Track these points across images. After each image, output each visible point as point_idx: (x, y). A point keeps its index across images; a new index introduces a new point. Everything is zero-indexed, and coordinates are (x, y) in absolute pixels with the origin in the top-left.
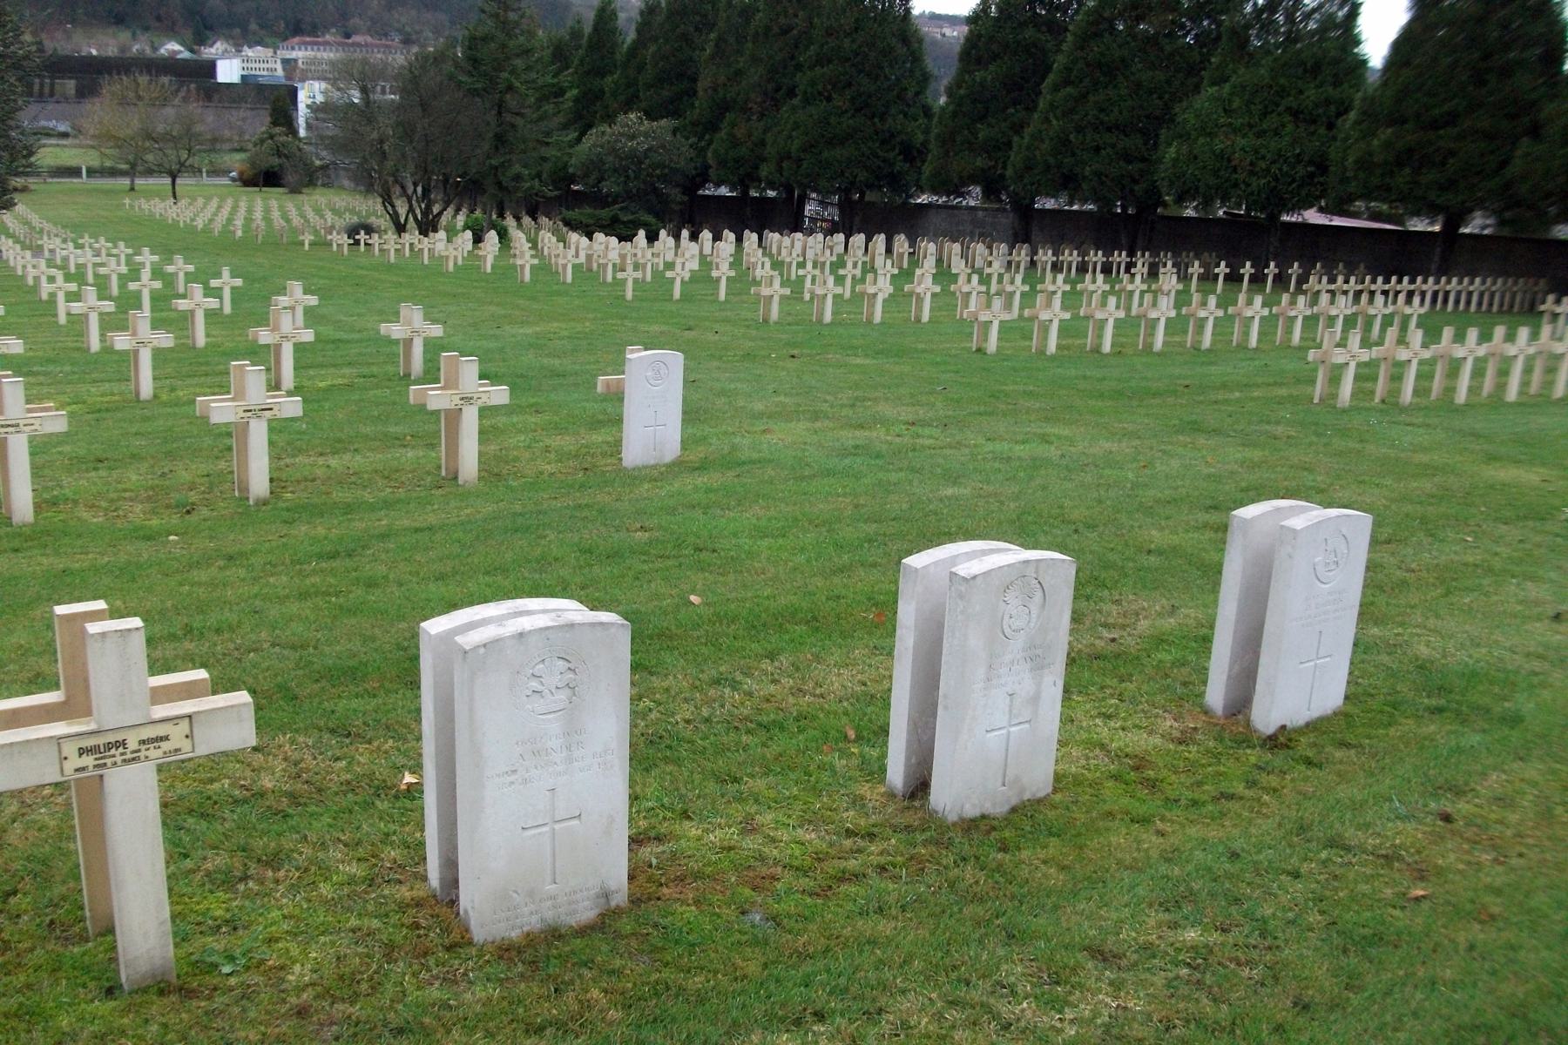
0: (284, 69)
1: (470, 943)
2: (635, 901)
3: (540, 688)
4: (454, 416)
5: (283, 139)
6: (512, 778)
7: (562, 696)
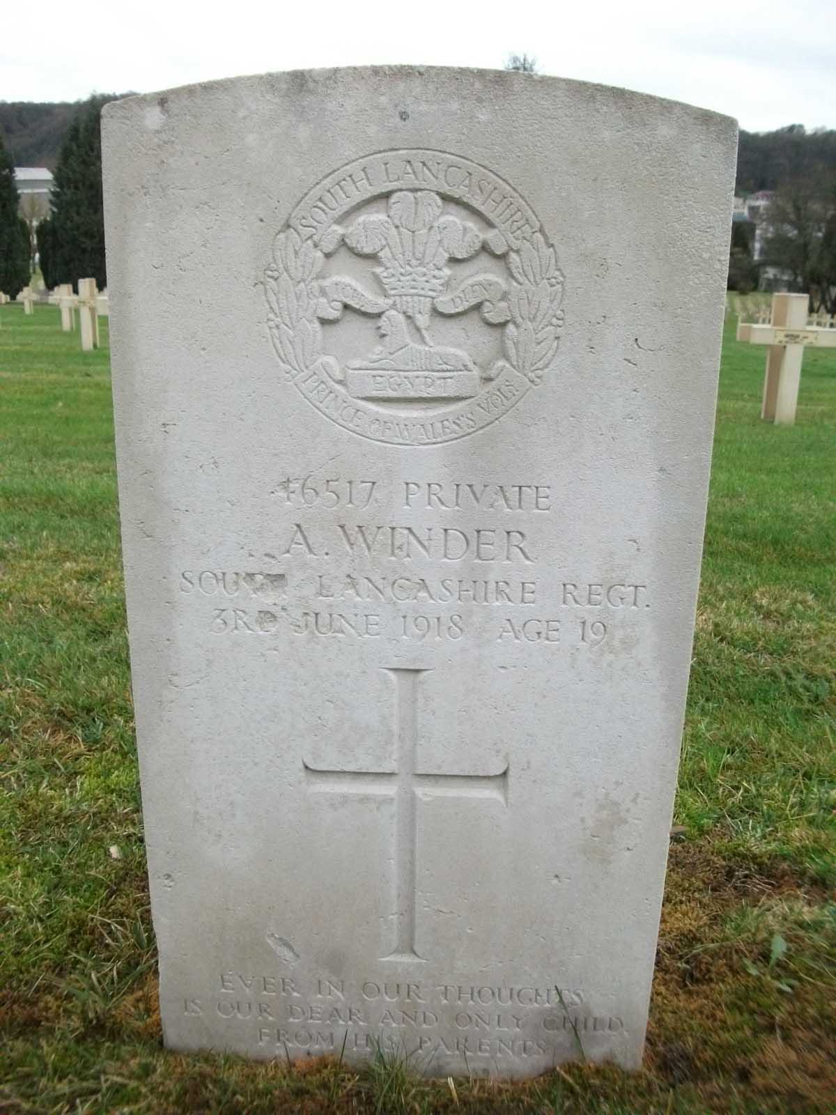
0: (749, 213)
1: (155, 1040)
2: (671, 1058)
3: (370, 299)
4: (777, 354)
5: (740, 256)
6: (268, 599)
7: (459, 346)
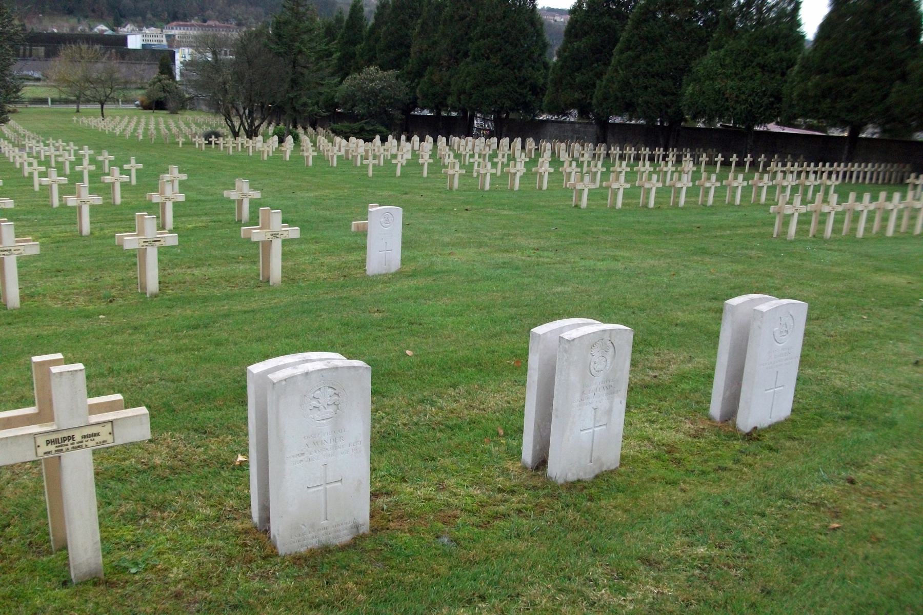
0: (167, 41)
1: (277, 555)
2: (374, 530)
3: (318, 405)
4: (267, 245)
5: (166, 82)
6: (302, 458)
7: (331, 409)
